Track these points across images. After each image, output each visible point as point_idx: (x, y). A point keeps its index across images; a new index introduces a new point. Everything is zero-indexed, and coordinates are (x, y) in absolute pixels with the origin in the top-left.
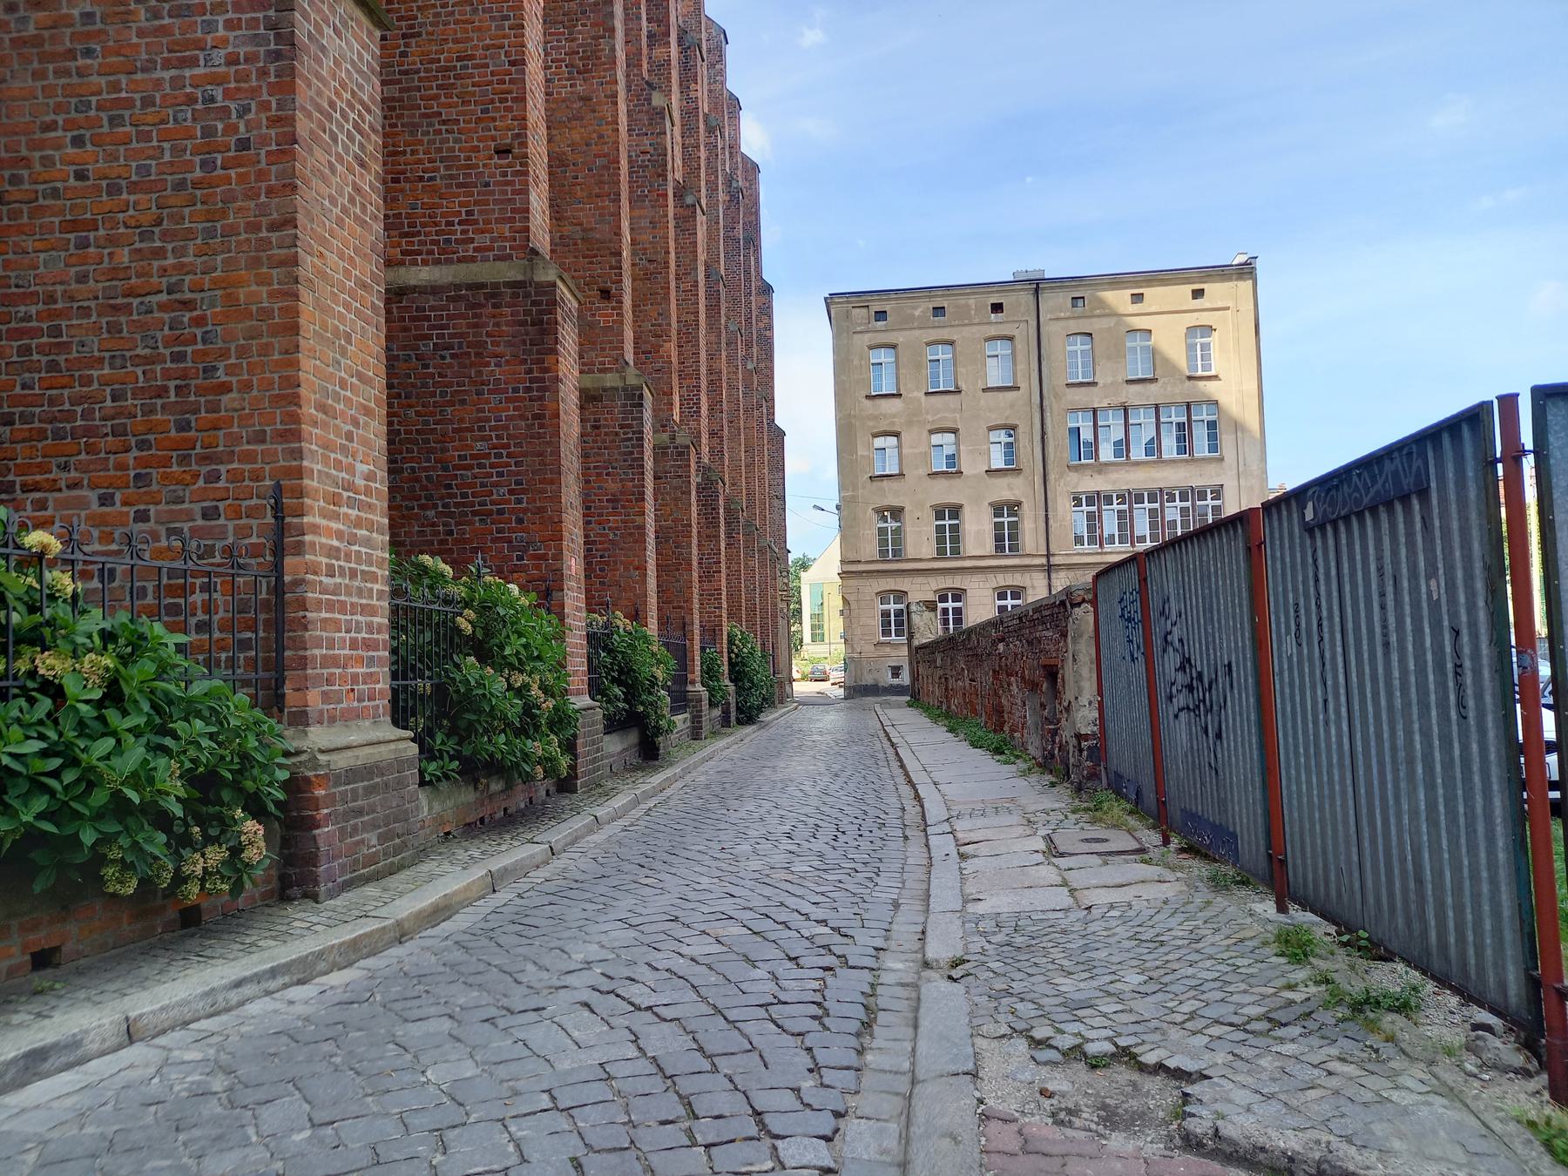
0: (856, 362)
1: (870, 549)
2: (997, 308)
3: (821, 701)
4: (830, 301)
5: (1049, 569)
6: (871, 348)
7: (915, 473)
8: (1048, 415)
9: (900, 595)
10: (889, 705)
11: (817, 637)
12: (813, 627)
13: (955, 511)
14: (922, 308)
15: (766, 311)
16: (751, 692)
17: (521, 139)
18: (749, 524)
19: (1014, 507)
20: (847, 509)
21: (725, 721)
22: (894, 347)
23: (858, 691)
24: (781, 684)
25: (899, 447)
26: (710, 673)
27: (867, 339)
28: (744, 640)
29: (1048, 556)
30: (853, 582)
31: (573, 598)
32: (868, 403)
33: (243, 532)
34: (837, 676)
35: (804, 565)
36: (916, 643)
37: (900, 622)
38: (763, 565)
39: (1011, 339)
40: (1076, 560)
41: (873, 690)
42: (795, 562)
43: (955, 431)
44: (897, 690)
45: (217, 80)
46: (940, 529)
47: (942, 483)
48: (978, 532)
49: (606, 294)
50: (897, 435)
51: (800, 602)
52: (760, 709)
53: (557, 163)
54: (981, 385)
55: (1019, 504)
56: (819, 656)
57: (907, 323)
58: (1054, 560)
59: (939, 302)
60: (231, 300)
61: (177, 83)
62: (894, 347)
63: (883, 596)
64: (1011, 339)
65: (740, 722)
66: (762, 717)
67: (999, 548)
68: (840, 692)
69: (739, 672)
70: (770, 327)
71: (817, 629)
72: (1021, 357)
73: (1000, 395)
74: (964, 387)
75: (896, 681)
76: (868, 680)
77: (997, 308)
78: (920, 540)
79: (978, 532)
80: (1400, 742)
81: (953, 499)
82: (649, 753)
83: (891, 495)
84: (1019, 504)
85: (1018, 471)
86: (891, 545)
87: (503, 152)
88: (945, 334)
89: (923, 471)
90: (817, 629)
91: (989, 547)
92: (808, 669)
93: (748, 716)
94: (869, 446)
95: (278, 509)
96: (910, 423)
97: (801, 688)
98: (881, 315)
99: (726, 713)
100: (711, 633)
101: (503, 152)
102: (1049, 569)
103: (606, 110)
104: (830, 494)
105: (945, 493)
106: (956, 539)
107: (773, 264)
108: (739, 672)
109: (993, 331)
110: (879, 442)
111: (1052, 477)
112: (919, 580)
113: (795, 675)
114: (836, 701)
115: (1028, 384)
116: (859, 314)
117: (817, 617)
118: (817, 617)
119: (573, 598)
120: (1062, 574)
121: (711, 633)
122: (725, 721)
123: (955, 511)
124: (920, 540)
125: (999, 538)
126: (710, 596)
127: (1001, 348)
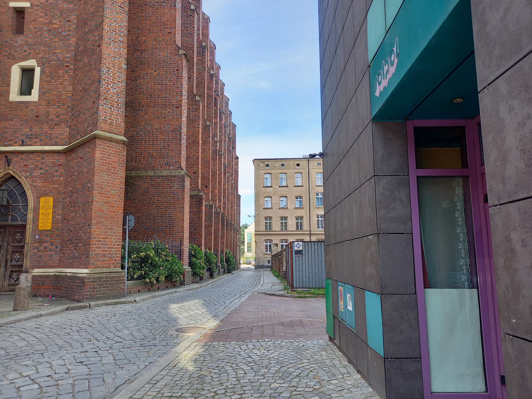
0: (260, 177)
1: (263, 228)
2: (298, 165)
3: (249, 269)
4: (254, 161)
5: (310, 235)
6: (265, 174)
7: (276, 208)
8: (311, 194)
9: (271, 241)
10: (266, 270)
11: (249, 250)
12: (248, 247)
13: (286, 218)
14: (278, 164)
15: (237, 164)
16: (231, 265)
17: (198, 171)
18: (231, 224)
19: (301, 218)
20: (257, 217)
21: (224, 272)
22: (271, 174)
23: (258, 267)
24: (237, 264)
25: (272, 200)
26: (222, 261)
27: (264, 171)
28: (229, 253)
29: (310, 231)
30: (258, 237)
31: (203, 247)
32: (264, 188)
33: (176, 243)
34: (253, 263)
35: (246, 227)
36: (273, 254)
37: (269, 248)
38: (234, 233)
39: (302, 173)
40: (317, 233)
41: (262, 267)
42: (243, 226)
43: (286, 197)
44: (268, 267)
45: (175, 190)
46: (282, 223)
47: (282, 210)
48: (292, 224)
49: (206, 187)
50: (271, 197)
51: (244, 239)
52: (232, 270)
53: (202, 176)
54: (294, 185)
55: (303, 217)
56: (248, 257)
57: (274, 168)
58: (312, 232)
59: (283, 162)
60: (176, 216)
61: (170, 191)
62: (271, 174)
63: (266, 241)
64: (302, 173)
65: (227, 273)
66: (232, 272)
67: (297, 228)
68: (254, 267)
69: (227, 261)
70: (238, 168)
71: (249, 247)
72: (304, 178)
73: (298, 188)
74: (289, 185)
75: (269, 264)
76: (261, 264)
77: (298, 165)
78: (276, 226)
79: (292, 224)
80: (297, 268)
81: (285, 215)
82: (211, 276)
83: (269, 213)
84: (303, 217)
85: (303, 208)
86: (269, 227)
87: (195, 173)
88: (284, 171)
89: (278, 207)
90: (249, 247)
91: (295, 229)
92: (245, 261)
93: (229, 271)
94: (263, 200)
95: (181, 241)
96: (274, 194)
97: (242, 266)
98: (267, 165)
99: (224, 270)
100: (222, 252)
101: (195, 173)
102: (310, 235)
103: (208, 152)
104: (252, 212)
105: (283, 213)
106: (286, 226)
107: (239, 152)
108: (227, 261)
109: (297, 171)
110: (266, 199)
111: (311, 210)
112: (276, 237)
113: (241, 262)
114: (253, 269)
115: (306, 185)
116: (262, 164)
117: (249, 244)
118: (249, 244)
119: (203, 247)
120: (314, 236)
121: (222, 252)
122: (224, 272)
123: (286, 218)
124: (276, 226)
125: (297, 226)
126: (223, 243)
127: (299, 175)
